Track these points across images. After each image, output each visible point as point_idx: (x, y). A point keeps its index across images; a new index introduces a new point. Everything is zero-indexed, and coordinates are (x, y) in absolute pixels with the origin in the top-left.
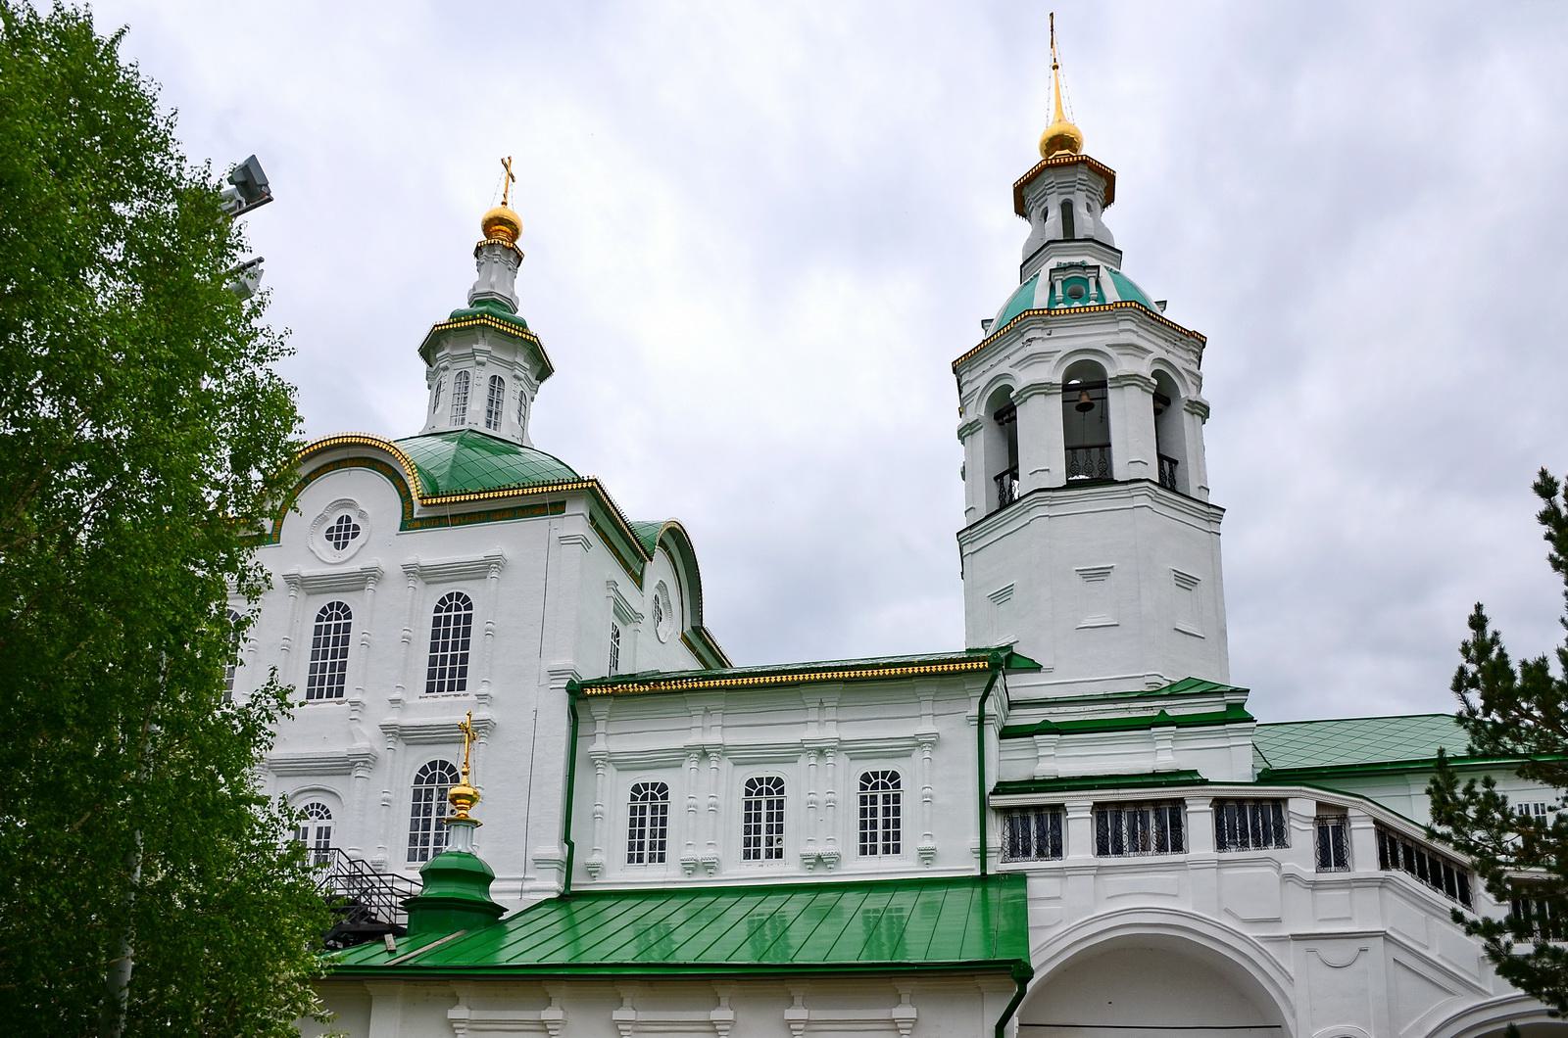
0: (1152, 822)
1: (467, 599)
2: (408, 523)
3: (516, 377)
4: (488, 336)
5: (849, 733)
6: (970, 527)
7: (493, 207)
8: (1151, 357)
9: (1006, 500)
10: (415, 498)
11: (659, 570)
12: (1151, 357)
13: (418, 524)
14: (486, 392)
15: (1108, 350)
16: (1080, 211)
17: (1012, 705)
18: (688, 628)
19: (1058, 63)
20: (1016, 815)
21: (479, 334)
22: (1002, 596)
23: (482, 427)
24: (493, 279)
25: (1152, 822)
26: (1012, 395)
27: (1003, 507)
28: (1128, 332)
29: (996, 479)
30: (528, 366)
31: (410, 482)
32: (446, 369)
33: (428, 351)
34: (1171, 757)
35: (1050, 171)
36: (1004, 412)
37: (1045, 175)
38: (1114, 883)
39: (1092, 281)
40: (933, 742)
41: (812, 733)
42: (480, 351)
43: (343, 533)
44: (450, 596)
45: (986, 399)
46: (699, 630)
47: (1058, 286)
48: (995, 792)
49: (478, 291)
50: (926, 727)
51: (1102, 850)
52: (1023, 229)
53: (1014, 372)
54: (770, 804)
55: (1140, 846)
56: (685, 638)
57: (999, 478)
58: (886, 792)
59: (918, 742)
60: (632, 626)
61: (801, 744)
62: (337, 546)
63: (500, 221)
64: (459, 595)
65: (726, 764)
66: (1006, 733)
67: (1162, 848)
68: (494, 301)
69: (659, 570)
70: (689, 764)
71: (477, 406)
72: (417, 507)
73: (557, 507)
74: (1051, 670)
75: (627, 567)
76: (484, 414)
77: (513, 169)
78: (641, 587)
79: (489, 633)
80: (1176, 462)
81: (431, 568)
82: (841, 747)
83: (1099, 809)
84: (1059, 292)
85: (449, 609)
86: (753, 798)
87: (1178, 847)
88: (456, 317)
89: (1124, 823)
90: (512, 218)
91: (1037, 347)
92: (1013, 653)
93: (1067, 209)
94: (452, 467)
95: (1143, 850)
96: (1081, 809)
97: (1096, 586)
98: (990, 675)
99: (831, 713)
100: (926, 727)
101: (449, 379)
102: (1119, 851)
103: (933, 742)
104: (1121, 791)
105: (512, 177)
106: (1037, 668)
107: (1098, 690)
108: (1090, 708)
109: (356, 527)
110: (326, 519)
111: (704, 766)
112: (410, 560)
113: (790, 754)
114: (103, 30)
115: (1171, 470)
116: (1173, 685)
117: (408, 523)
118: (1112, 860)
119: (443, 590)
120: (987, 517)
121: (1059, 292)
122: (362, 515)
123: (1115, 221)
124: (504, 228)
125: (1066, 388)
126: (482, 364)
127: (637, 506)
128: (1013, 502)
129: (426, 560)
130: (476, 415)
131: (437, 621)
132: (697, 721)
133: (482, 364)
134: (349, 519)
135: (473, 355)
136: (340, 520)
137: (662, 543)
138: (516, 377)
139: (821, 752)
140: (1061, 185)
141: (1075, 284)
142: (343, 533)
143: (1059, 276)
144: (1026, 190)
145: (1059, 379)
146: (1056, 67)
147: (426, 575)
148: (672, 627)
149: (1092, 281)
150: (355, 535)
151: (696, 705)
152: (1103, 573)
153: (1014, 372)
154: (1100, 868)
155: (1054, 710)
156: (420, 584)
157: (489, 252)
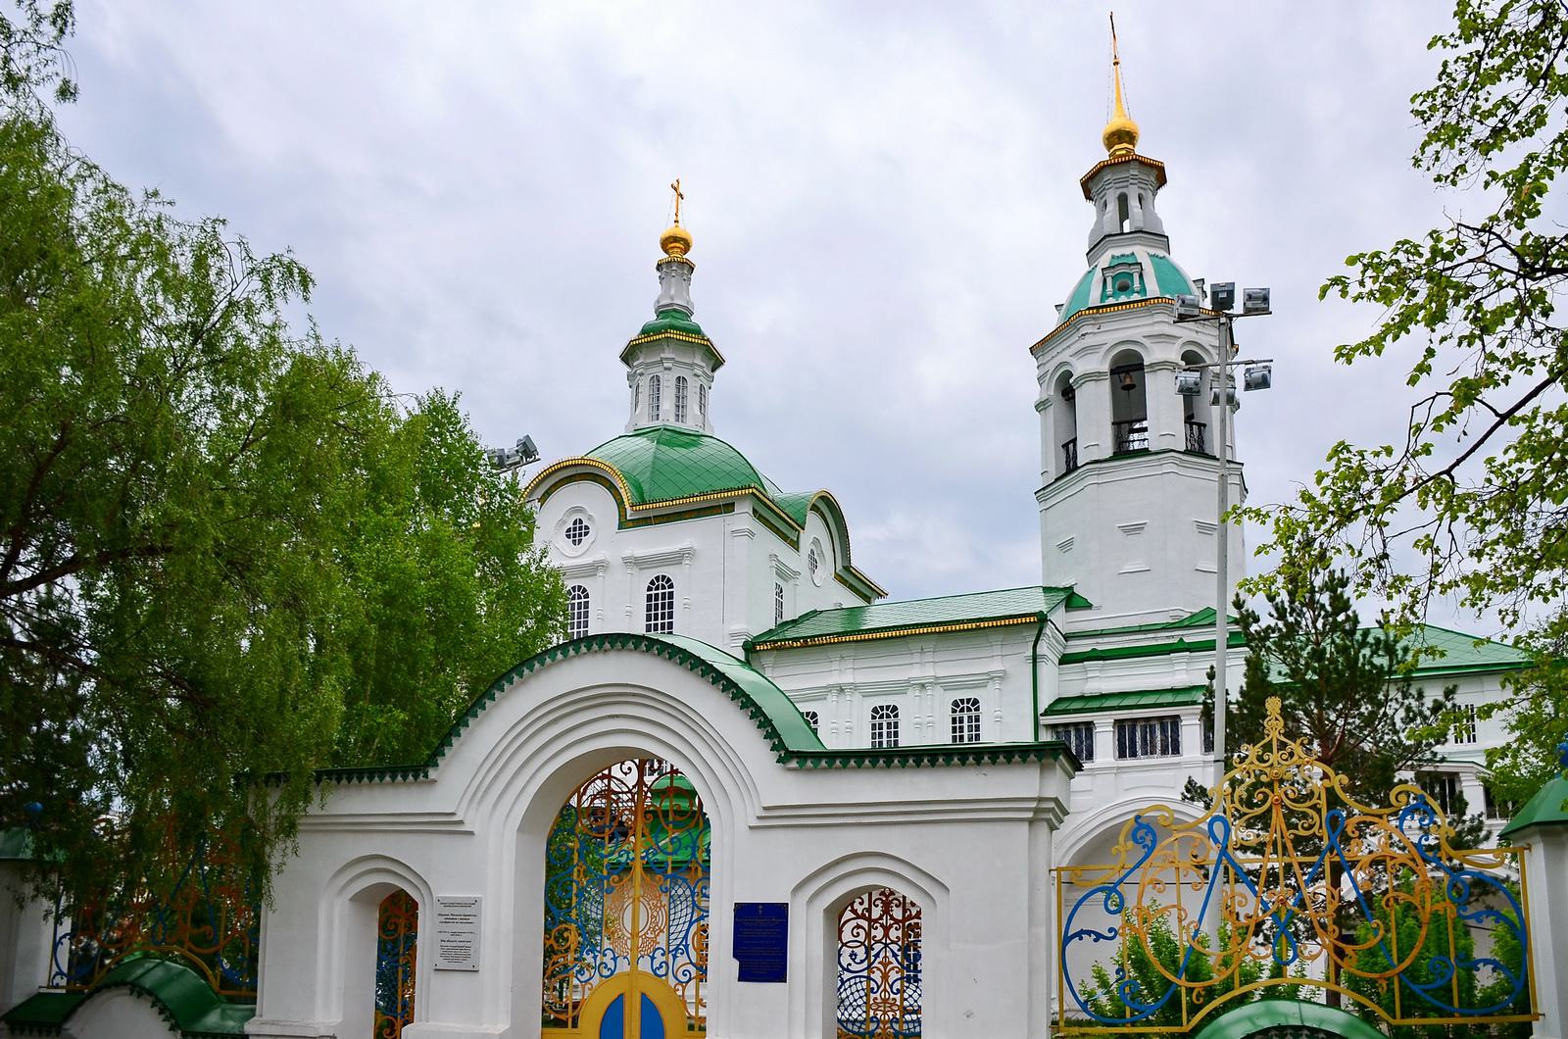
0: (1158, 733)
1: (669, 580)
2: (624, 524)
3: (695, 375)
4: (672, 346)
5: (942, 671)
6: (1044, 489)
7: (668, 229)
8: (1180, 342)
9: (1072, 466)
10: (627, 506)
11: (814, 529)
12: (1180, 342)
13: (631, 524)
14: (674, 390)
15: (1144, 341)
16: (1133, 203)
17: (1067, 637)
18: (839, 567)
19: (1120, 60)
20: (1060, 729)
21: (664, 344)
22: (1066, 546)
23: (672, 423)
24: (672, 292)
25: (1158, 733)
26: (1071, 381)
27: (1069, 471)
28: (1163, 323)
29: (1063, 446)
30: (704, 364)
31: (619, 485)
32: (641, 374)
33: (628, 356)
34: (1185, 676)
35: (1108, 170)
36: (1068, 393)
37: (1104, 173)
38: (1128, 779)
39: (1136, 277)
40: (1002, 676)
41: (916, 672)
42: (666, 359)
43: (577, 532)
44: (657, 578)
45: (1053, 385)
46: (847, 568)
47: (1109, 280)
48: (1046, 713)
49: (662, 303)
50: (996, 665)
51: (1122, 755)
52: (1086, 215)
53: (1072, 360)
54: (889, 724)
55: (1149, 750)
56: (839, 578)
57: (1065, 446)
58: (970, 714)
59: (991, 677)
60: (791, 582)
61: (908, 681)
62: (574, 542)
63: (675, 239)
64: (664, 577)
65: (857, 696)
66: (1065, 660)
67: (1164, 752)
68: (675, 310)
69: (814, 529)
70: (832, 698)
71: (667, 405)
72: (629, 512)
73: (729, 507)
74: (1099, 608)
75: (785, 538)
76: (674, 408)
77: (681, 190)
78: (643, 995)
79: (686, 606)
80: (1205, 425)
81: (643, 558)
82: (937, 681)
83: (1120, 724)
84: (1109, 289)
85: (657, 588)
86: (877, 721)
87: (1176, 751)
88: (645, 332)
89: (1138, 735)
90: (683, 235)
91: (1089, 341)
92: (1073, 593)
93: (1123, 200)
94: (652, 473)
95: (1152, 753)
96: (1105, 725)
97: (1134, 538)
98: (1038, 626)
99: (929, 657)
100: (996, 665)
101: (645, 383)
102: (1134, 755)
103: (1002, 676)
104: (1134, 711)
105: (681, 196)
106: (1090, 606)
107: (1135, 622)
108: (1127, 638)
109: (587, 527)
110: (565, 522)
111: (842, 698)
112: (627, 553)
113: (901, 688)
114: (449, 395)
115: (1200, 433)
116: (1193, 615)
117: (624, 524)
118: (1129, 762)
119: (652, 574)
120: (1057, 480)
121: (1109, 289)
122: (590, 518)
123: (1166, 205)
124: (678, 245)
125: (1113, 372)
126: (670, 369)
127: (787, 483)
128: (1076, 468)
129: (639, 552)
130: (668, 416)
131: (649, 598)
132: (835, 666)
133: (670, 369)
134: (581, 522)
135: (661, 361)
136: (575, 523)
137: (814, 508)
138: (695, 375)
139: (923, 686)
140: (1117, 181)
141: (1122, 277)
142: (577, 532)
143: (1110, 274)
144: (1090, 185)
145: (1106, 367)
146: (1116, 63)
147: (639, 563)
148: (826, 571)
149: (1136, 277)
150: (586, 534)
151: (834, 654)
152: (1139, 528)
153: (1072, 360)
154: (1119, 768)
155: (1100, 640)
156: (636, 569)
157: (667, 268)
